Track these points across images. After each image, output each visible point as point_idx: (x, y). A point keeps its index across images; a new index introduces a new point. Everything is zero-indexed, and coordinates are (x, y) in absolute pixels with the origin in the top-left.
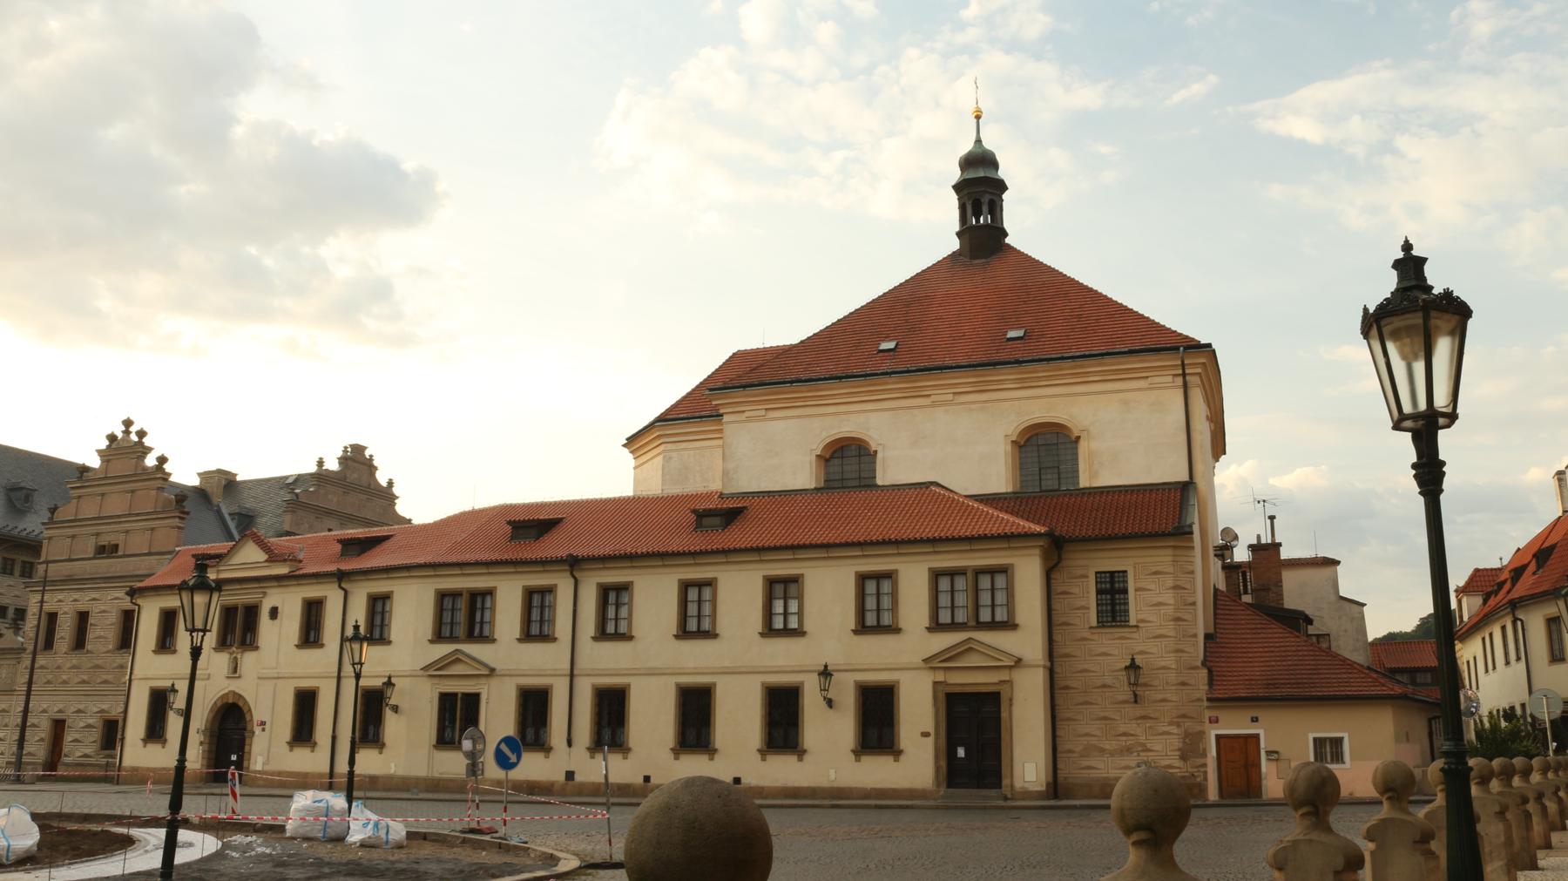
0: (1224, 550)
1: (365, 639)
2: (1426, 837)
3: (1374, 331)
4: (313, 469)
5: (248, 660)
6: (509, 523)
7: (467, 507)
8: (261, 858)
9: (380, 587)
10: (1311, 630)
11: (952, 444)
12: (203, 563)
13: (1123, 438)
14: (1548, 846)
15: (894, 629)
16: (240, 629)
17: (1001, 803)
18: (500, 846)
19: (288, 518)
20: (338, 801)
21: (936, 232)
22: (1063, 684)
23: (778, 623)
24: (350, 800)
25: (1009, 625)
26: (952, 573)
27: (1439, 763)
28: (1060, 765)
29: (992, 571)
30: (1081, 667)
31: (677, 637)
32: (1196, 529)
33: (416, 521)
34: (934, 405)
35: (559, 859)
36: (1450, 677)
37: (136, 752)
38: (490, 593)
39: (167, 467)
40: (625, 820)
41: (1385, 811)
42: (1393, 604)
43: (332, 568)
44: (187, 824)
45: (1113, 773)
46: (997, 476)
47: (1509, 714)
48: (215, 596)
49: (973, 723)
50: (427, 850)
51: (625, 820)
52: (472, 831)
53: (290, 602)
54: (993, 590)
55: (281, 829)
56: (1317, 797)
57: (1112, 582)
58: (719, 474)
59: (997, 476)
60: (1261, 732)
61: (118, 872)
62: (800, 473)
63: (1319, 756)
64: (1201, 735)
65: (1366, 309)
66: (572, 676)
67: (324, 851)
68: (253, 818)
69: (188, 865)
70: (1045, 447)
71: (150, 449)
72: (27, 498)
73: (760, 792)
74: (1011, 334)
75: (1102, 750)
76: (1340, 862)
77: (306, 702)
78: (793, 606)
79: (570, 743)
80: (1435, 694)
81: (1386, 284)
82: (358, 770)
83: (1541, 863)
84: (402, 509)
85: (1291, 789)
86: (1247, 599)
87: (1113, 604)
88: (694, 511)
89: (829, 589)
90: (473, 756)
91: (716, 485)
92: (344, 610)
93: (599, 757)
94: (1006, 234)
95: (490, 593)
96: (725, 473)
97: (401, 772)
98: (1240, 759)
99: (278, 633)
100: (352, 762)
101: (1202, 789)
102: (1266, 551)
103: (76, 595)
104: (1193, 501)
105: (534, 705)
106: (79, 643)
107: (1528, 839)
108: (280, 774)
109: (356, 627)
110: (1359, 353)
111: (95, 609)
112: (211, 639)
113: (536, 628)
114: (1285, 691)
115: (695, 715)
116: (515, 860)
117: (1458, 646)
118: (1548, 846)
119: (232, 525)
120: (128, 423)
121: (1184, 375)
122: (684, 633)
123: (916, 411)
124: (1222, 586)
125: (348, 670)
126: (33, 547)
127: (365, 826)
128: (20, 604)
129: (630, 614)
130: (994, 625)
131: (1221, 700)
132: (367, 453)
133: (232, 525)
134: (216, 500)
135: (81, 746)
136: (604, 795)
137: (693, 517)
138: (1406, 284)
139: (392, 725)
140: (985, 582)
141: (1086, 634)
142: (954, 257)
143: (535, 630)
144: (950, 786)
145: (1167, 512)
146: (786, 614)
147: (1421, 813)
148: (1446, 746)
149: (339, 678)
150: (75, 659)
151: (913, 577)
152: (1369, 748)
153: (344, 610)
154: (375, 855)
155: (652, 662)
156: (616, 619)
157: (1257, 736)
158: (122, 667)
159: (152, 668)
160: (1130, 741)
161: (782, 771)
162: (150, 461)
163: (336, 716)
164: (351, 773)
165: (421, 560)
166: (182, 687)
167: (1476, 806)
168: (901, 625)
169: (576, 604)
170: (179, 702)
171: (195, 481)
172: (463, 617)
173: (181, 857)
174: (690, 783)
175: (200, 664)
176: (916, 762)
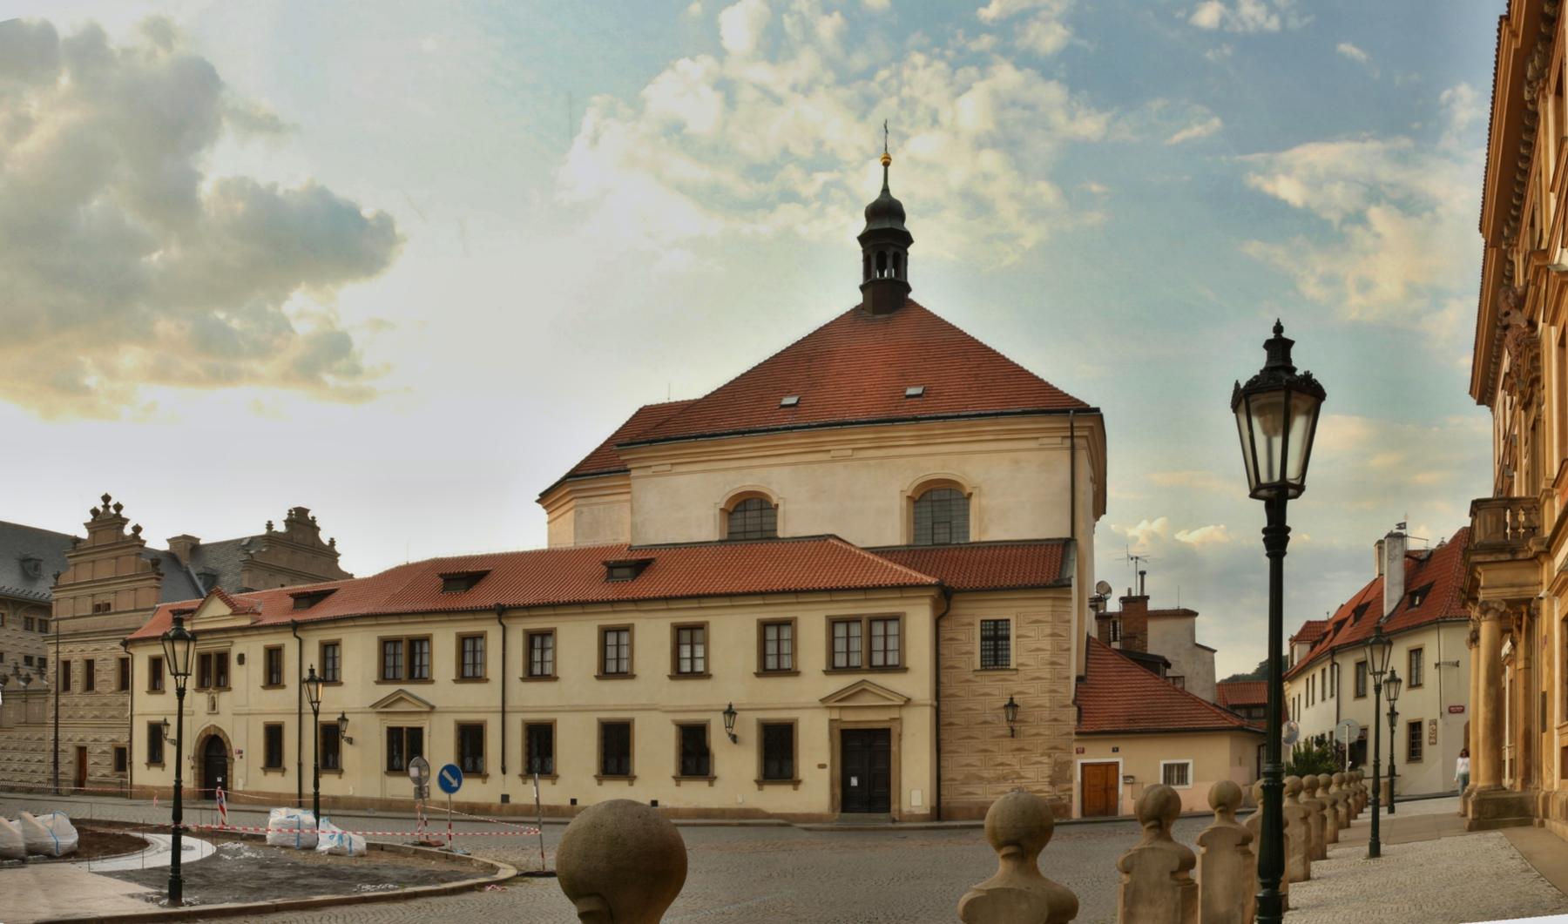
0: (1098, 602)
1: (320, 680)
2: (1246, 840)
3: (1243, 406)
4: (264, 531)
5: (224, 699)
6: (441, 575)
7: (403, 563)
8: (248, 861)
9: (330, 635)
10: (1169, 673)
11: (848, 497)
12: (179, 617)
13: (1011, 494)
14: (1336, 840)
15: (793, 672)
16: (215, 672)
17: (890, 825)
18: (447, 857)
19: (246, 576)
20: (308, 817)
21: (841, 291)
22: (948, 721)
23: (686, 667)
24: (317, 816)
25: (900, 668)
26: (848, 621)
27: (1261, 782)
28: (943, 792)
29: (886, 619)
30: (964, 706)
31: (598, 677)
32: (1074, 582)
33: (357, 576)
34: (834, 460)
35: (498, 869)
36: (1277, 711)
37: (142, 774)
38: (427, 639)
39: (142, 535)
40: (556, 837)
41: (1216, 822)
42: (1237, 652)
43: (287, 619)
44: (187, 831)
45: (990, 798)
46: (894, 533)
47: (1320, 741)
48: (192, 645)
49: (865, 757)
50: (384, 859)
51: (556, 837)
52: (422, 844)
53: (253, 649)
54: (886, 636)
55: (262, 838)
56: (1162, 813)
57: (996, 630)
58: (627, 527)
59: (894, 533)
60: (1120, 760)
61: (139, 867)
62: (703, 525)
63: (1168, 779)
64: (1069, 764)
65: (1237, 384)
66: (503, 712)
67: (299, 857)
68: (239, 829)
69: (191, 864)
70: (938, 503)
71: (126, 521)
72: (36, 567)
73: (676, 813)
74: (911, 391)
75: (981, 779)
76: (1176, 864)
77: (274, 735)
78: (699, 651)
79: (504, 771)
80: (1262, 726)
81: (1254, 362)
82: (322, 791)
83: (1329, 854)
84: (344, 564)
85: (1140, 808)
86: (1116, 645)
87: (996, 650)
88: (605, 563)
89: (732, 635)
90: (419, 781)
91: (625, 538)
92: (301, 655)
93: (531, 783)
94: (909, 289)
95: (427, 639)
96: (634, 526)
97: (358, 794)
98: (1101, 783)
99: (247, 676)
100: (316, 785)
101: (1067, 809)
102: (1136, 603)
103: (83, 646)
104: (1073, 556)
105: (471, 738)
106: (89, 685)
107: (1322, 837)
108: (258, 793)
109: (312, 671)
110: (1227, 420)
111: (98, 657)
112: (191, 682)
113: (469, 669)
114: (1143, 725)
115: (616, 749)
116: (461, 869)
117: (1286, 685)
118: (1336, 840)
119: (200, 584)
120: (106, 498)
121: (1072, 437)
122: (604, 674)
123: (815, 466)
124: (1094, 634)
125: (307, 707)
126: (45, 607)
127: (331, 837)
128: (42, 654)
129: (555, 657)
130: (886, 669)
131: (1087, 734)
132: (310, 515)
133: (200, 584)
134: (185, 562)
135: (101, 768)
136: (536, 815)
137: (604, 569)
138: (1273, 364)
139: (348, 754)
140: (878, 629)
141: (971, 677)
142: (856, 311)
143: (469, 672)
144: (844, 810)
145: (1049, 566)
146: (692, 658)
147: (1244, 821)
148: (1266, 767)
149: (300, 714)
150: (87, 698)
151: (812, 624)
152: (1211, 768)
153: (301, 655)
154: (342, 861)
155: (576, 699)
156: (542, 662)
157: (1116, 764)
158: (124, 705)
159: (148, 706)
160: (1007, 770)
161: (695, 795)
162: (128, 531)
163: (300, 746)
164: (316, 794)
165: (364, 611)
166: (173, 721)
167: (1286, 814)
168: (800, 668)
169: (503, 646)
170: (172, 733)
171: (165, 547)
172: (404, 662)
173: (186, 858)
174: (613, 805)
175: (185, 702)
176: (814, 787)
